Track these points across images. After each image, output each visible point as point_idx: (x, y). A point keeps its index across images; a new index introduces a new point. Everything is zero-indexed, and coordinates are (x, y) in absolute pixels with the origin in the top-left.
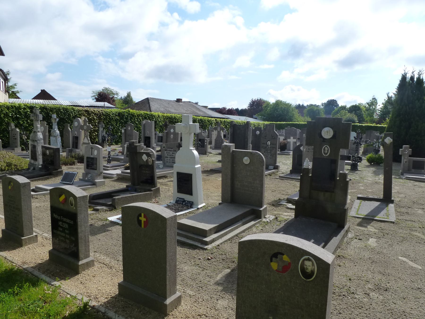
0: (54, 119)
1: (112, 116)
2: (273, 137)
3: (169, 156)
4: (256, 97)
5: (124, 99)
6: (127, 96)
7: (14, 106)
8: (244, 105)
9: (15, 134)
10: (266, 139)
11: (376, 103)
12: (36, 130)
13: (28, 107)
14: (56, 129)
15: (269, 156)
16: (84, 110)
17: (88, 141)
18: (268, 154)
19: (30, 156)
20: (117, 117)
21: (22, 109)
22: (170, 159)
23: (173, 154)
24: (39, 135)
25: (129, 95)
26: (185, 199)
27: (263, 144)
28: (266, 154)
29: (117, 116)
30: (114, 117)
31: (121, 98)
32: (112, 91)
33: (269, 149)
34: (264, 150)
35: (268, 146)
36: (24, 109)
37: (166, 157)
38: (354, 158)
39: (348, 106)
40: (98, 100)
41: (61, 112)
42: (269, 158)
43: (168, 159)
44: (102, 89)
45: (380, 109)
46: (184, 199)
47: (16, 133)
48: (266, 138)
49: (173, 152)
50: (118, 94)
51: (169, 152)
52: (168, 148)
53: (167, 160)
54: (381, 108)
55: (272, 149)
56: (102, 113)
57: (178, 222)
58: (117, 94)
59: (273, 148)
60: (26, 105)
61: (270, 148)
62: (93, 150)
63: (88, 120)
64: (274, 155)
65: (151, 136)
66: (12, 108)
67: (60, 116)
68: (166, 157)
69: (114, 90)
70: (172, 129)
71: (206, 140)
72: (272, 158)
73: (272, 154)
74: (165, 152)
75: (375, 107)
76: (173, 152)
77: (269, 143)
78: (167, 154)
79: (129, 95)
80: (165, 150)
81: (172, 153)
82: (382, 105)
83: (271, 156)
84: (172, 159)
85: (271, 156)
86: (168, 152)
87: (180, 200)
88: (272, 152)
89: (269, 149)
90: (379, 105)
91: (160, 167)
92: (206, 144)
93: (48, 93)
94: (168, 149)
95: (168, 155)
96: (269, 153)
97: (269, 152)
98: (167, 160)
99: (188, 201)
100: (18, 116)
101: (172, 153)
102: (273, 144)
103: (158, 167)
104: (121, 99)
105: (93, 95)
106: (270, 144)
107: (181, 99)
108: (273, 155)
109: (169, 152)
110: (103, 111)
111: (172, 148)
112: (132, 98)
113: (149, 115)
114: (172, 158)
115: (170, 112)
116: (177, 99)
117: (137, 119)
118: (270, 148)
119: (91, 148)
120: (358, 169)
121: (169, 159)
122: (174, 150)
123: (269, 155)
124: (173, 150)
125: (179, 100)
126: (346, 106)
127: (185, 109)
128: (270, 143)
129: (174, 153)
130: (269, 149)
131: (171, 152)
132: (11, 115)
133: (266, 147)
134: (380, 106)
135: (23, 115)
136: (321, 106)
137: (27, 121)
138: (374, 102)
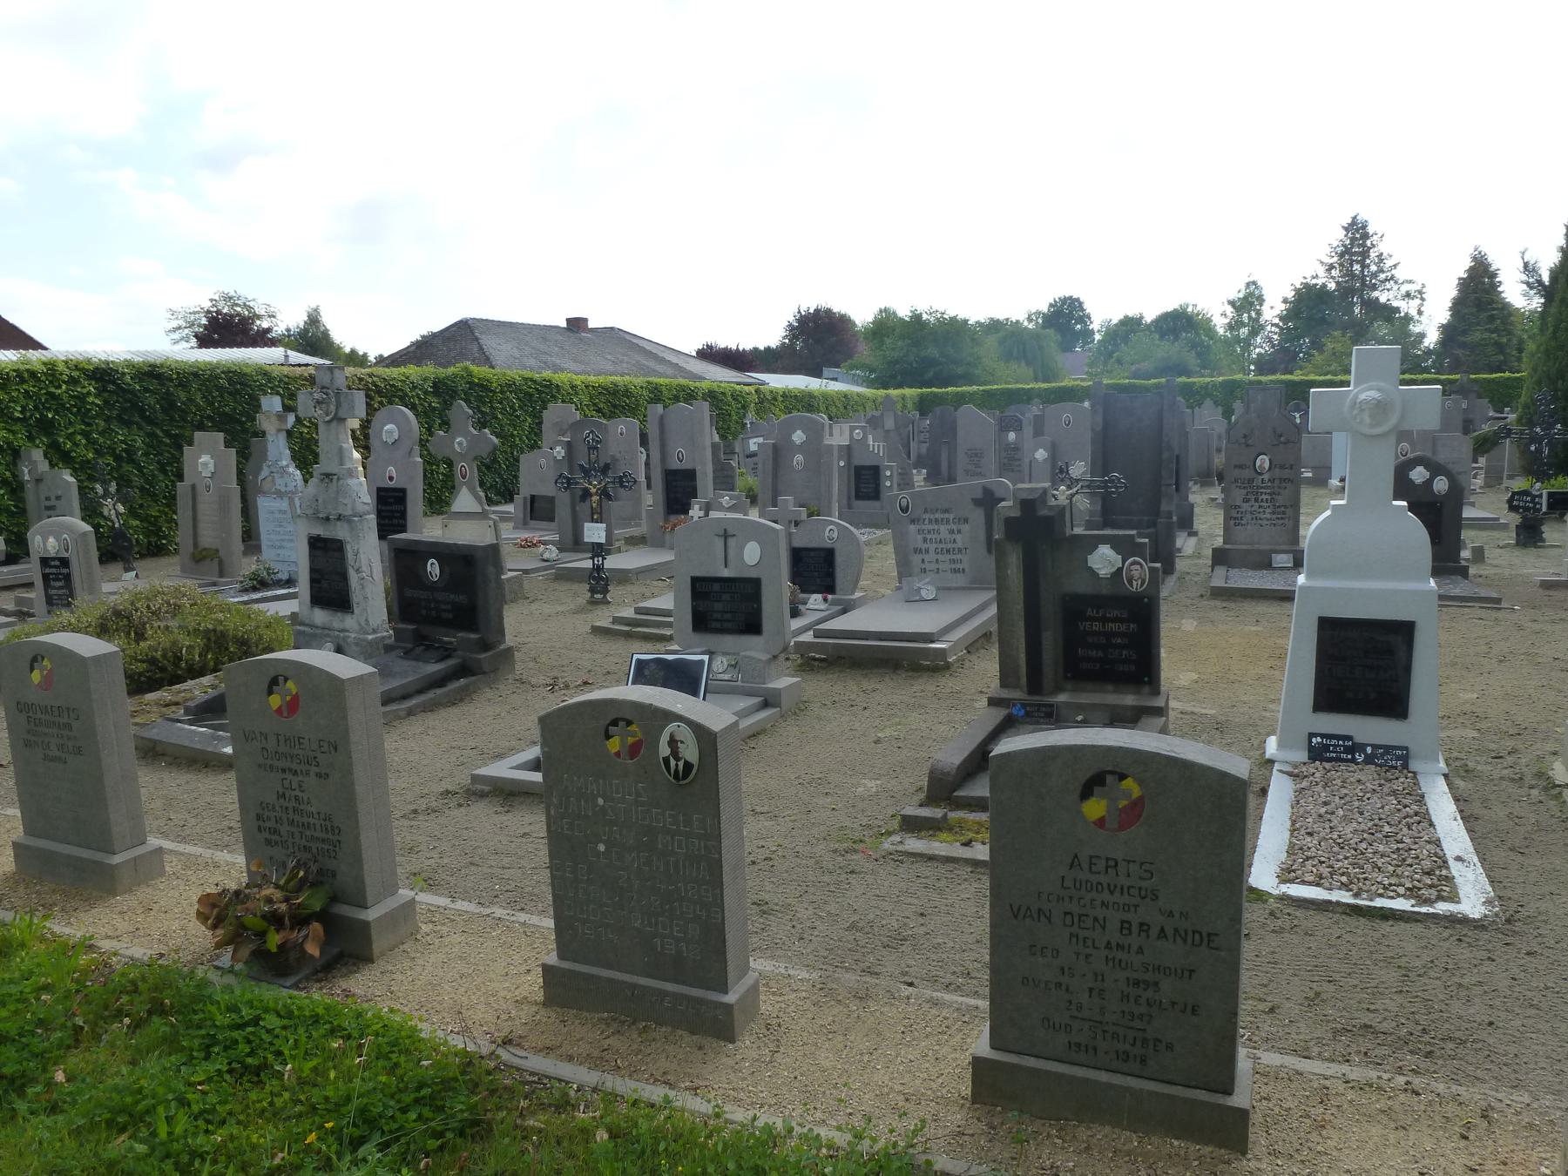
0: (273, 419)
1: (413, 396)
2: (1281, 436)
3: (932, 547)
4: (810, 304)
5: (299, 334)
6: (305, 322)
7: (28, 370)
8: (769, 334)
9: (58, 498)
10: (1248, 446)
11: (1261, 300)
12: (332, 467)
13: (88, 376)
14: (284, 463)
15: (1268, 516)
16: (306, 375)
17: (481, 504)
18: (1260, 507)
19: (303, 587)
20: (430, 398)
21: (64, 382)
22: (940, 557)
23: (954, 536)
24: (355, 488)
25: (314, 319)
26: (1359, 739)
27: (1236, 466)
28: (1253, 509)
29: (426, 393)
30: (420, 398)
31: (288, 330)
32: (251, 304)
33: (1262, 488)
34: (1245, 491)
35: (1261, 474)
36: (73, 381)
37: (917, 551)
38: (1529, 498)
39: (1149, 317)
40: (204, 341)
41: (220, 389)
42: (1265, 522)
43: (926, 557)
44: (211, 300)
45: (1276, 321)
46: (1349, 738)
47: (60, 493)
48: (1250, 442)
49: (954, 527)
50: (274, 317)
51: (931, 527)
52: (926, 511)
53: (923, 561)
54: (1281, 318)
55: (1279, 487)
56: (374, 384)
57: (478, 775)
58: (270, 316)
59: (1282, 480)
60: (76, 366)
61: (1269, 484)
62: (731, 542)
63: (470, 411)
64: (1289, 512)
65: (698, 468)
66: (23, 381)
67: (220, 406)
68: (917, 551)
69: (260, 301)
70: (799, 432)
71: (890, 468)
72: (1281, 522)
73: (1279, 507)
74: (912, 528)
75: (1259, 313)
76: (954, 527)
77: (1263, 461)
78: (920, 537)
79: (314, 319)
80: (913, 521)
81: (952, 532)
82: (1283, 307)
83: (1275, 516)
84: (949, 557)
85: (1274, 513)
86: (924, 527)
87: (1335, 746)
88: (1280, 500)
89: (1267, 487)
90: (1272, 308)
91: (924, 593)
92: (888, 484)
93: (7, 322)
94: (927, 516)
95: (925, 540)
96: (1265, 504)
97: (1264, 497)
98: (923, 561)
99: (1374, 747)
100: (50, 416)
101: (952, 532)
102: (1282, 467)
103: (917, 598)
104: (289, 336)
105: (175, 324)
106: (1267, 465)
107: (585, 320)
108: (1283, 509)
109: (931, 527)
110: (375, 379)
111: (946, 511)
112: (327, 330)
113: (540, 384)
114: (948, 551)
115: (557, 369)
116: (567, 320)
117: (501, 403)
118: (1269, 484)
119: (722, 533)
120: (1543, 540)
121: (932, 556)
122: (959, 519)
123: (1268, 510)
124: (951, 517)
125: (576, 324)
126: (1141, 318)
127: (609, 357)
128: (1270, 460)
129: (959, 532)
130: (1267, 487)
131: (943, 528)
132: (21, 412)
133: (1251, 481)
134: (1272, 310)
135: (68, 409)
136: (1026, 323)
137: (86, 435)
138: (1249, 302)
